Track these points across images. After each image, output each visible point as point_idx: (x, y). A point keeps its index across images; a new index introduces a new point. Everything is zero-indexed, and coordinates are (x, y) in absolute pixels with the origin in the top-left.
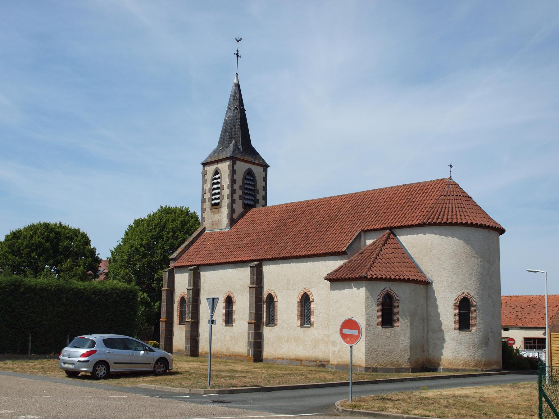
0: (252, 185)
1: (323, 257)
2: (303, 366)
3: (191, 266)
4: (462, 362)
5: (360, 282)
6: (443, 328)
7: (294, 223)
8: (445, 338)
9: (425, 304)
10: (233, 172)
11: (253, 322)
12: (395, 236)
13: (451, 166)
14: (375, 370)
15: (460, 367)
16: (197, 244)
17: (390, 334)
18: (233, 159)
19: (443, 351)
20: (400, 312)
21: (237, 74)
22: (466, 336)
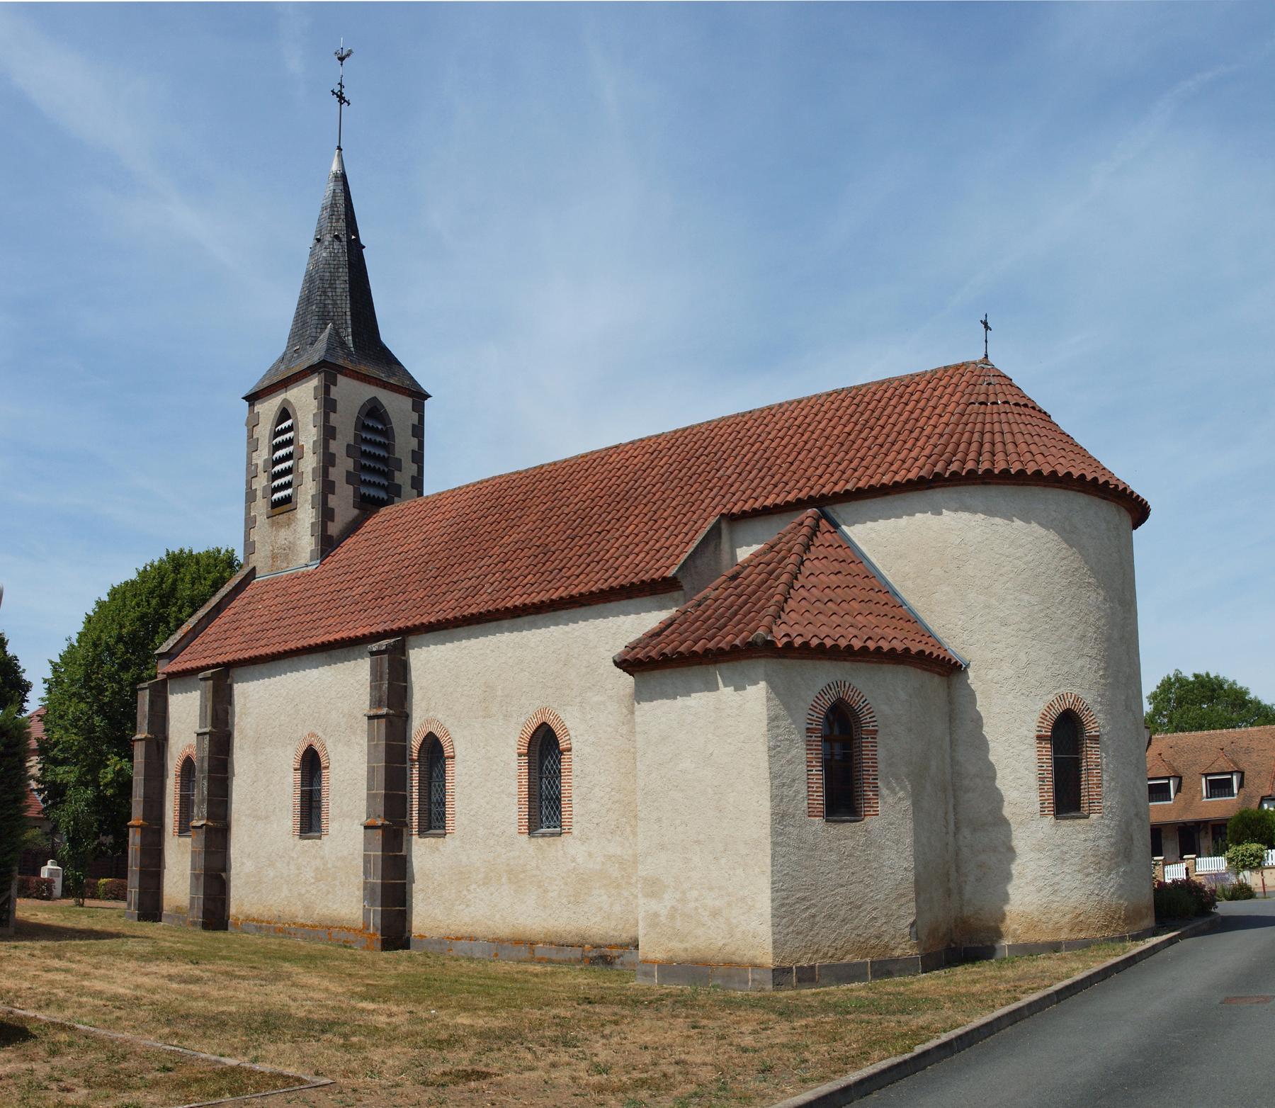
0: (379, 445)
1: (600, 607)
2: (540, 961)
5: (745, 663)
6: (1007, 812)
8: (1015, 843)
9: (948, 739)
10: (328, 405)
11: (379, 822)
12: (836, 526)
14: (807, 976)
15: (1063, 936)
16: (233, 611)
17: (851, 843)
18: (328, 370)
19: (1011, 889)
20: (881, 766)
21: (339, 148)
22: (1088, 834)
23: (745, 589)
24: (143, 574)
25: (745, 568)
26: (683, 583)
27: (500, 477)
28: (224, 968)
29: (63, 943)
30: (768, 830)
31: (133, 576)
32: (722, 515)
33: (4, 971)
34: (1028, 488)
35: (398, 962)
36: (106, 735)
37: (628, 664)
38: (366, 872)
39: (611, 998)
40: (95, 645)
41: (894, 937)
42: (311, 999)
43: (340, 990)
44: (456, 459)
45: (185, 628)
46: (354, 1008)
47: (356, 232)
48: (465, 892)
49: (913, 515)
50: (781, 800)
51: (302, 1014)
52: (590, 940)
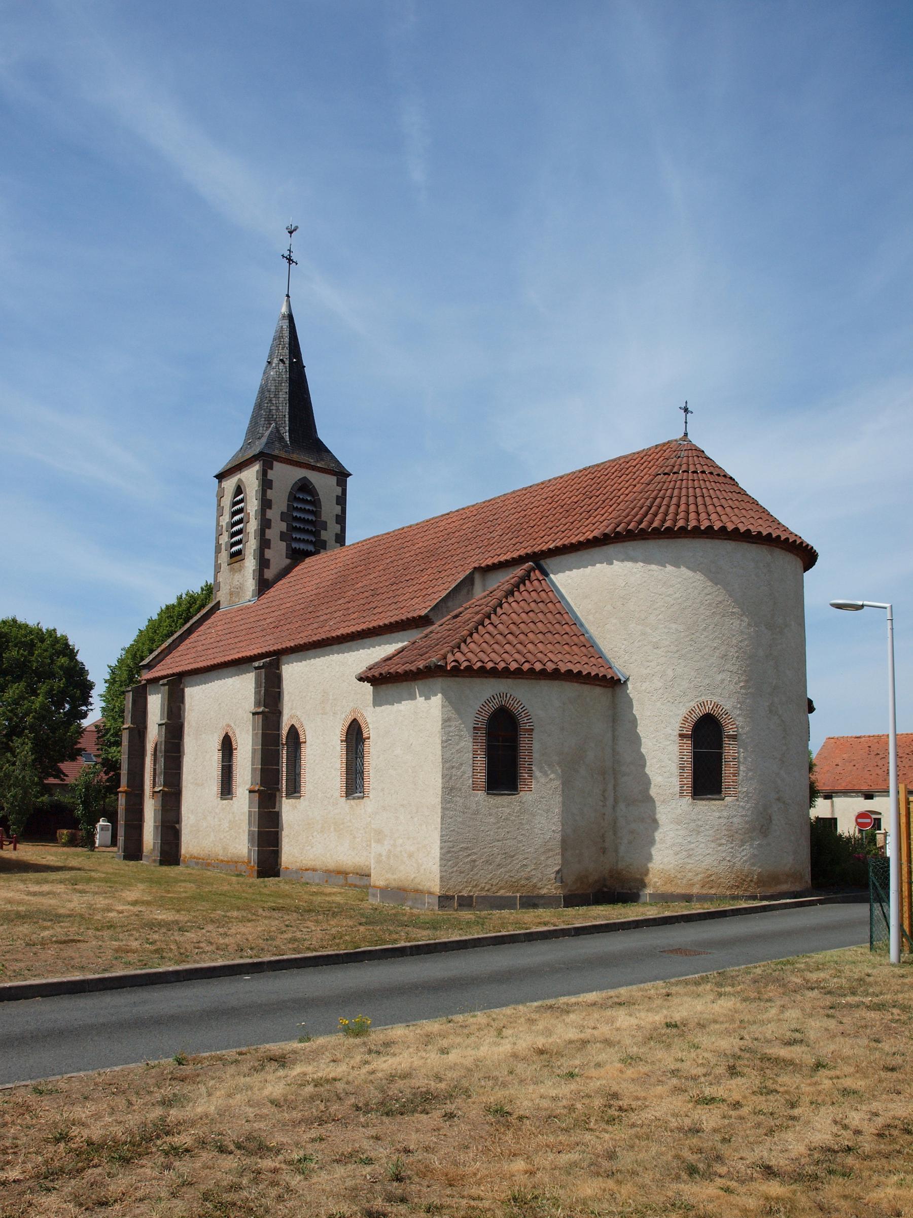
0: (309, 512)
4: (699, 877)
6: (653, 792)
8: (658, 816)
10: (266, 484)
12: (545, 574)
13: (686, 410)
14: (466, 902)
15: (695, 890)
17: (507, 810)
18: (266, 459)
19: (654, 851)
21: (288, 296)
30: (439, 799)
32: (475, 568)
34: (679, 540)
41: (541, 880)
44: (368, 517)
49: (594, 565)
50: (451, 778)
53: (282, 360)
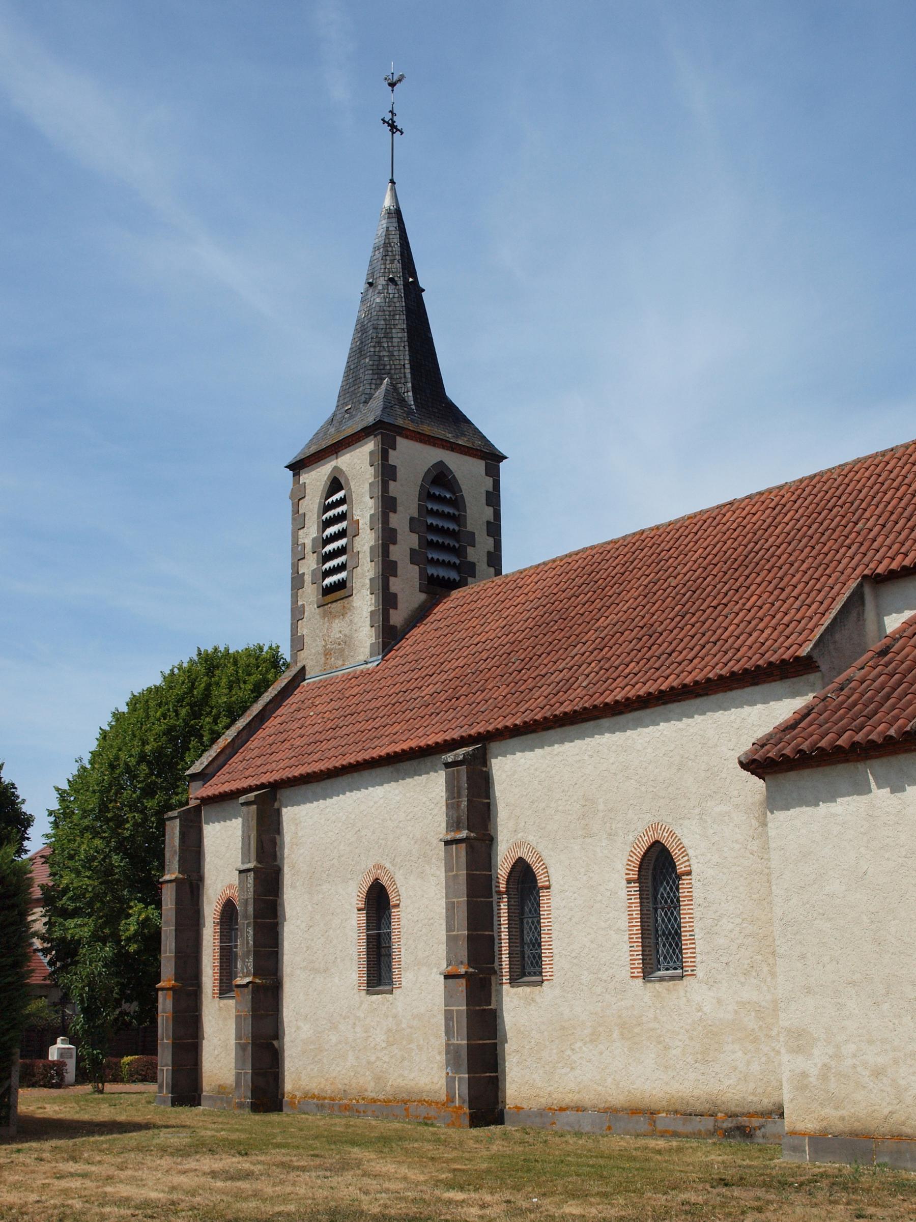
1: (720, 696)
2: (663, 1135)
3: (250, 789)
5: (902, 758)
7: (598, 604)
10: (387, 473)
11: (462, 970)
16: (279, 720)
18: (385, 432)
21: (392, 182)
23: (898, 666)
24: (170, 679)
25: (896, 640)
26: (820, 663)
27: (592, 548)
28: (279, 1158)
29: (78, 1141)
31: (158, 681)
32: (865, 577)
33: (4, 1182)
35: (491, 1139)
36: (128, 878)
37: (755, 765)
38: (448, 1032)
39: (752, 1180)
40: (112, 767)
42: (387, 1191)
43: (422, 1178)
44: (543, 524)
45: (222, 742)
46: (439, 1200)
47: (413, 274)
48: (569, 1052)
51: (376, 1209)
52: (723, 1108)
53: (392, 280)
